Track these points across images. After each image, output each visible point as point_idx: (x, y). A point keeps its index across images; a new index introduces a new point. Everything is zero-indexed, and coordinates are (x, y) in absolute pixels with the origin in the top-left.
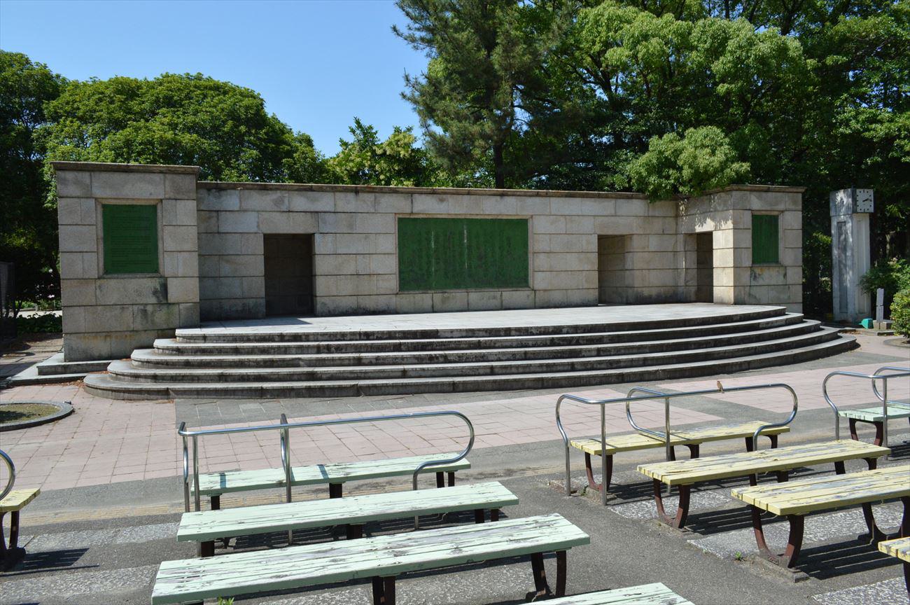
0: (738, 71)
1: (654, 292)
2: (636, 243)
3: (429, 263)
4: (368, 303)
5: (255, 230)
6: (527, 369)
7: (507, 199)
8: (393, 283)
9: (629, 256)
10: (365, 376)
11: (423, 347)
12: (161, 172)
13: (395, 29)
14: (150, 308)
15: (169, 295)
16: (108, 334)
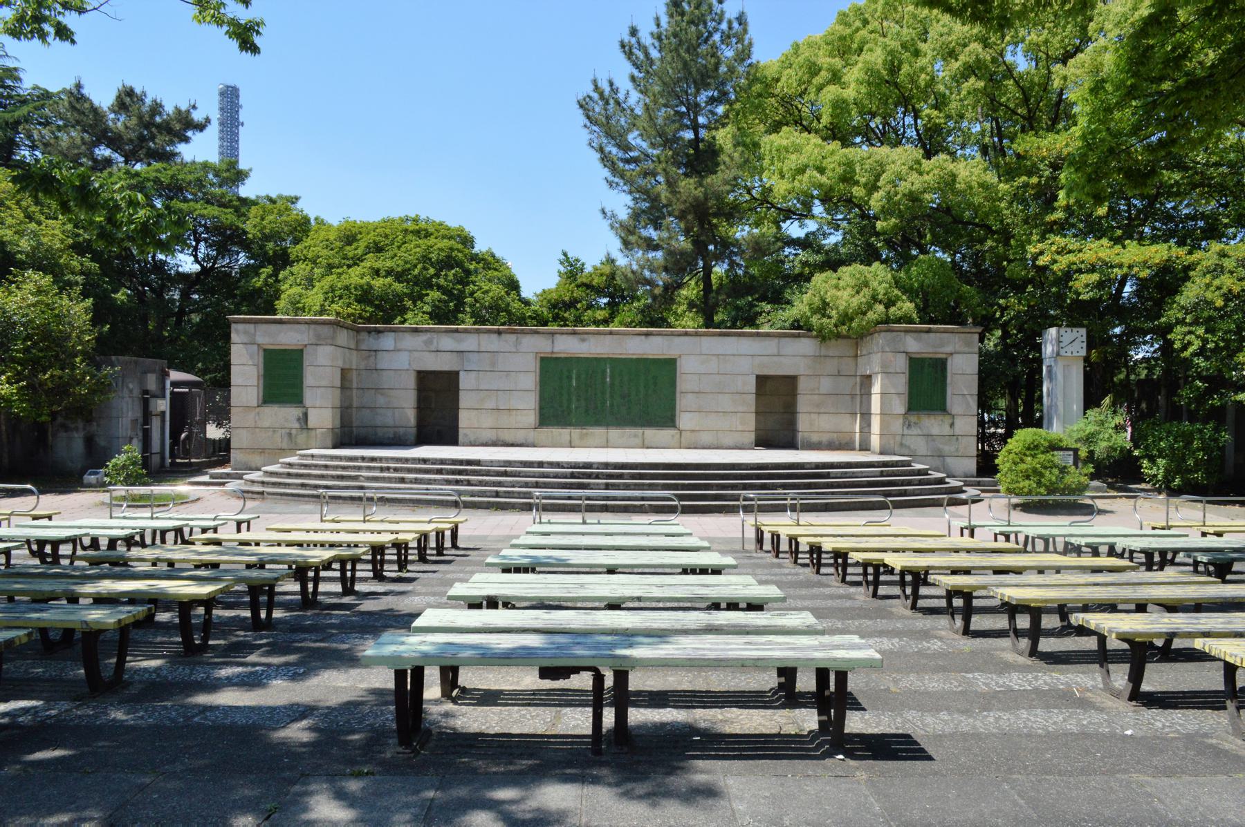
1: (825, 438)
3: (569, 401)
4: (507, 436)
7: (652, 338)
8: (531, 418)
14: (294, 432)
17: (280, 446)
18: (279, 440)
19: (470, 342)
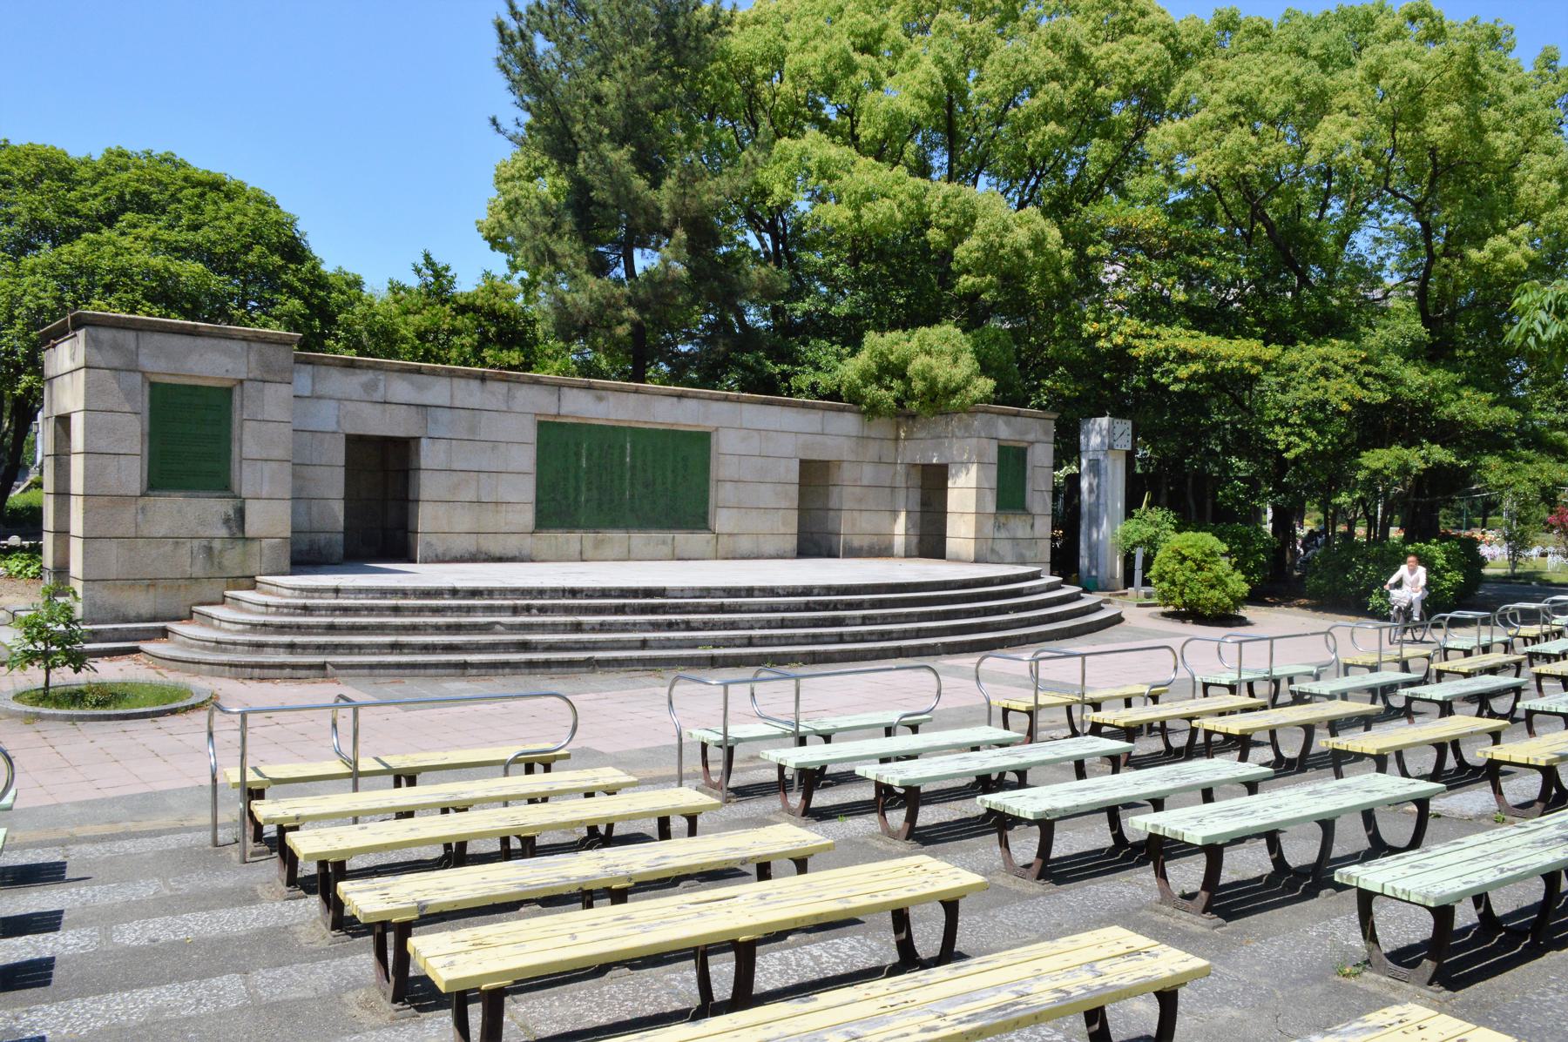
0: (990, 259)
2: (847, 474)
3: (577, 489)
4: (493, 545)
5: (333, 427)
6: (789, 640)
7: (687, 403)
8: (528, 517)
9: (835, 491)
10: (595, 646)
11: (654, 610)
12: (244, 339)
13: (494, 122)
14: (217, 545)
15: (247, 527)
16: (152, 583)
17: (188, 571)
18: (187, 561)
19: (438, 391)
